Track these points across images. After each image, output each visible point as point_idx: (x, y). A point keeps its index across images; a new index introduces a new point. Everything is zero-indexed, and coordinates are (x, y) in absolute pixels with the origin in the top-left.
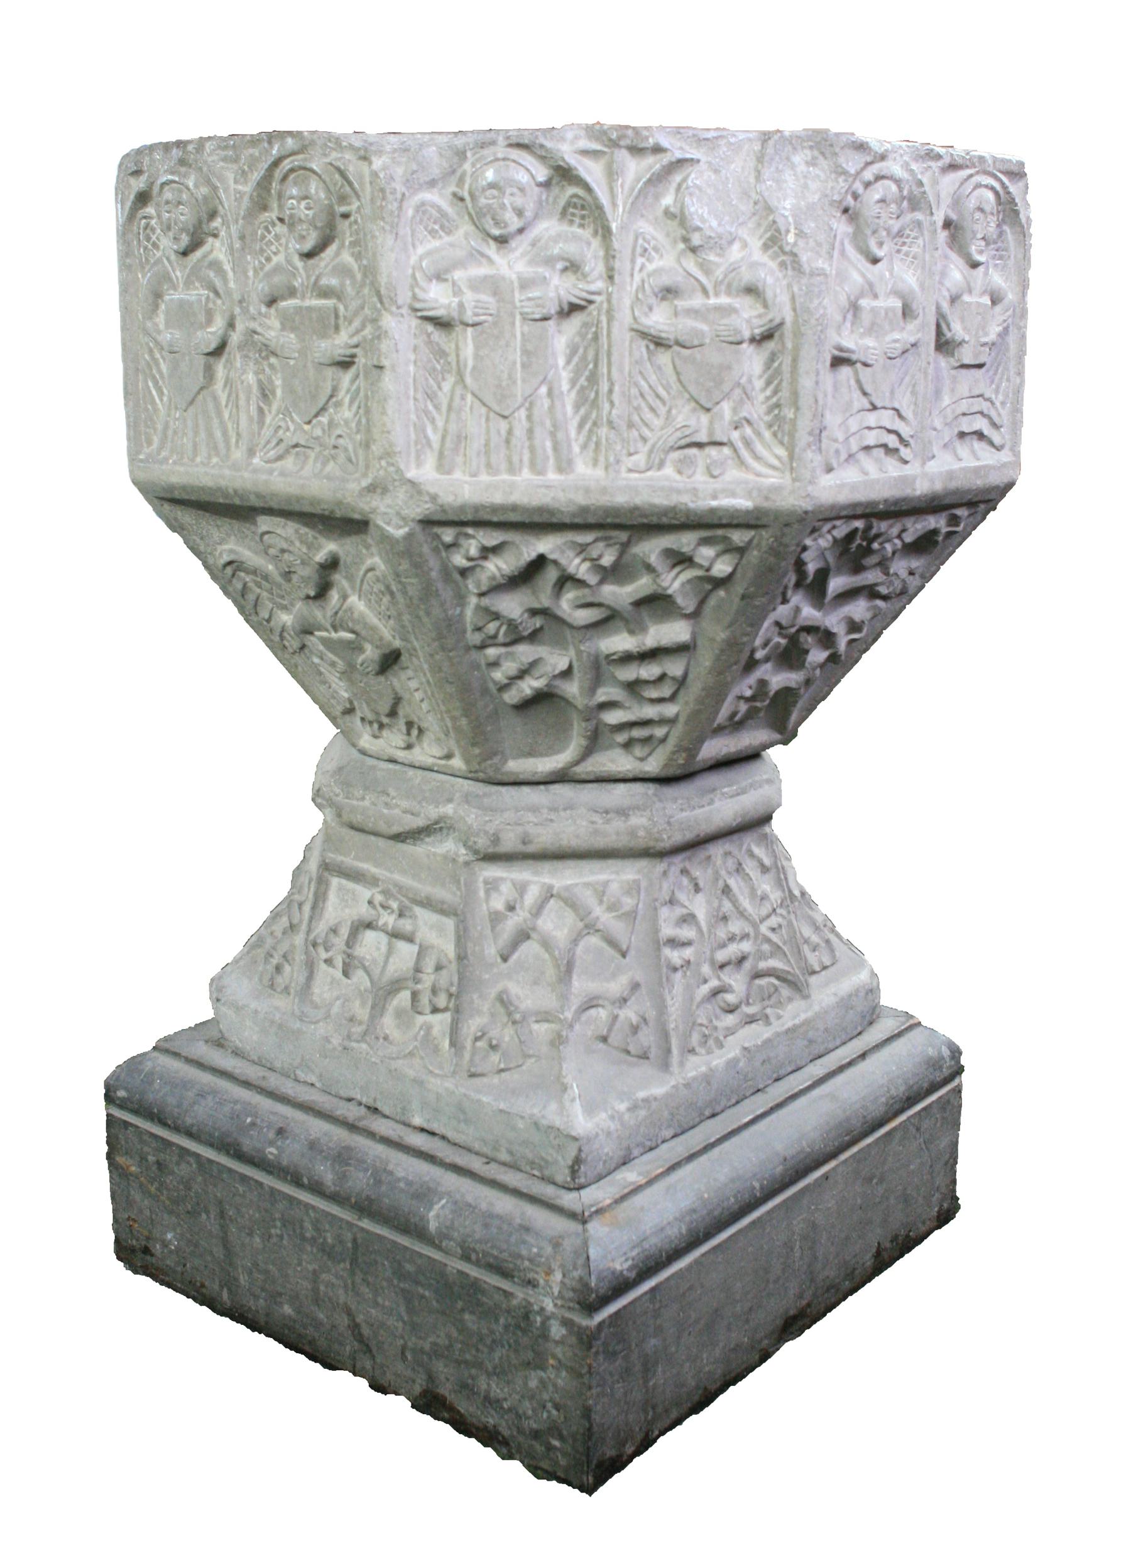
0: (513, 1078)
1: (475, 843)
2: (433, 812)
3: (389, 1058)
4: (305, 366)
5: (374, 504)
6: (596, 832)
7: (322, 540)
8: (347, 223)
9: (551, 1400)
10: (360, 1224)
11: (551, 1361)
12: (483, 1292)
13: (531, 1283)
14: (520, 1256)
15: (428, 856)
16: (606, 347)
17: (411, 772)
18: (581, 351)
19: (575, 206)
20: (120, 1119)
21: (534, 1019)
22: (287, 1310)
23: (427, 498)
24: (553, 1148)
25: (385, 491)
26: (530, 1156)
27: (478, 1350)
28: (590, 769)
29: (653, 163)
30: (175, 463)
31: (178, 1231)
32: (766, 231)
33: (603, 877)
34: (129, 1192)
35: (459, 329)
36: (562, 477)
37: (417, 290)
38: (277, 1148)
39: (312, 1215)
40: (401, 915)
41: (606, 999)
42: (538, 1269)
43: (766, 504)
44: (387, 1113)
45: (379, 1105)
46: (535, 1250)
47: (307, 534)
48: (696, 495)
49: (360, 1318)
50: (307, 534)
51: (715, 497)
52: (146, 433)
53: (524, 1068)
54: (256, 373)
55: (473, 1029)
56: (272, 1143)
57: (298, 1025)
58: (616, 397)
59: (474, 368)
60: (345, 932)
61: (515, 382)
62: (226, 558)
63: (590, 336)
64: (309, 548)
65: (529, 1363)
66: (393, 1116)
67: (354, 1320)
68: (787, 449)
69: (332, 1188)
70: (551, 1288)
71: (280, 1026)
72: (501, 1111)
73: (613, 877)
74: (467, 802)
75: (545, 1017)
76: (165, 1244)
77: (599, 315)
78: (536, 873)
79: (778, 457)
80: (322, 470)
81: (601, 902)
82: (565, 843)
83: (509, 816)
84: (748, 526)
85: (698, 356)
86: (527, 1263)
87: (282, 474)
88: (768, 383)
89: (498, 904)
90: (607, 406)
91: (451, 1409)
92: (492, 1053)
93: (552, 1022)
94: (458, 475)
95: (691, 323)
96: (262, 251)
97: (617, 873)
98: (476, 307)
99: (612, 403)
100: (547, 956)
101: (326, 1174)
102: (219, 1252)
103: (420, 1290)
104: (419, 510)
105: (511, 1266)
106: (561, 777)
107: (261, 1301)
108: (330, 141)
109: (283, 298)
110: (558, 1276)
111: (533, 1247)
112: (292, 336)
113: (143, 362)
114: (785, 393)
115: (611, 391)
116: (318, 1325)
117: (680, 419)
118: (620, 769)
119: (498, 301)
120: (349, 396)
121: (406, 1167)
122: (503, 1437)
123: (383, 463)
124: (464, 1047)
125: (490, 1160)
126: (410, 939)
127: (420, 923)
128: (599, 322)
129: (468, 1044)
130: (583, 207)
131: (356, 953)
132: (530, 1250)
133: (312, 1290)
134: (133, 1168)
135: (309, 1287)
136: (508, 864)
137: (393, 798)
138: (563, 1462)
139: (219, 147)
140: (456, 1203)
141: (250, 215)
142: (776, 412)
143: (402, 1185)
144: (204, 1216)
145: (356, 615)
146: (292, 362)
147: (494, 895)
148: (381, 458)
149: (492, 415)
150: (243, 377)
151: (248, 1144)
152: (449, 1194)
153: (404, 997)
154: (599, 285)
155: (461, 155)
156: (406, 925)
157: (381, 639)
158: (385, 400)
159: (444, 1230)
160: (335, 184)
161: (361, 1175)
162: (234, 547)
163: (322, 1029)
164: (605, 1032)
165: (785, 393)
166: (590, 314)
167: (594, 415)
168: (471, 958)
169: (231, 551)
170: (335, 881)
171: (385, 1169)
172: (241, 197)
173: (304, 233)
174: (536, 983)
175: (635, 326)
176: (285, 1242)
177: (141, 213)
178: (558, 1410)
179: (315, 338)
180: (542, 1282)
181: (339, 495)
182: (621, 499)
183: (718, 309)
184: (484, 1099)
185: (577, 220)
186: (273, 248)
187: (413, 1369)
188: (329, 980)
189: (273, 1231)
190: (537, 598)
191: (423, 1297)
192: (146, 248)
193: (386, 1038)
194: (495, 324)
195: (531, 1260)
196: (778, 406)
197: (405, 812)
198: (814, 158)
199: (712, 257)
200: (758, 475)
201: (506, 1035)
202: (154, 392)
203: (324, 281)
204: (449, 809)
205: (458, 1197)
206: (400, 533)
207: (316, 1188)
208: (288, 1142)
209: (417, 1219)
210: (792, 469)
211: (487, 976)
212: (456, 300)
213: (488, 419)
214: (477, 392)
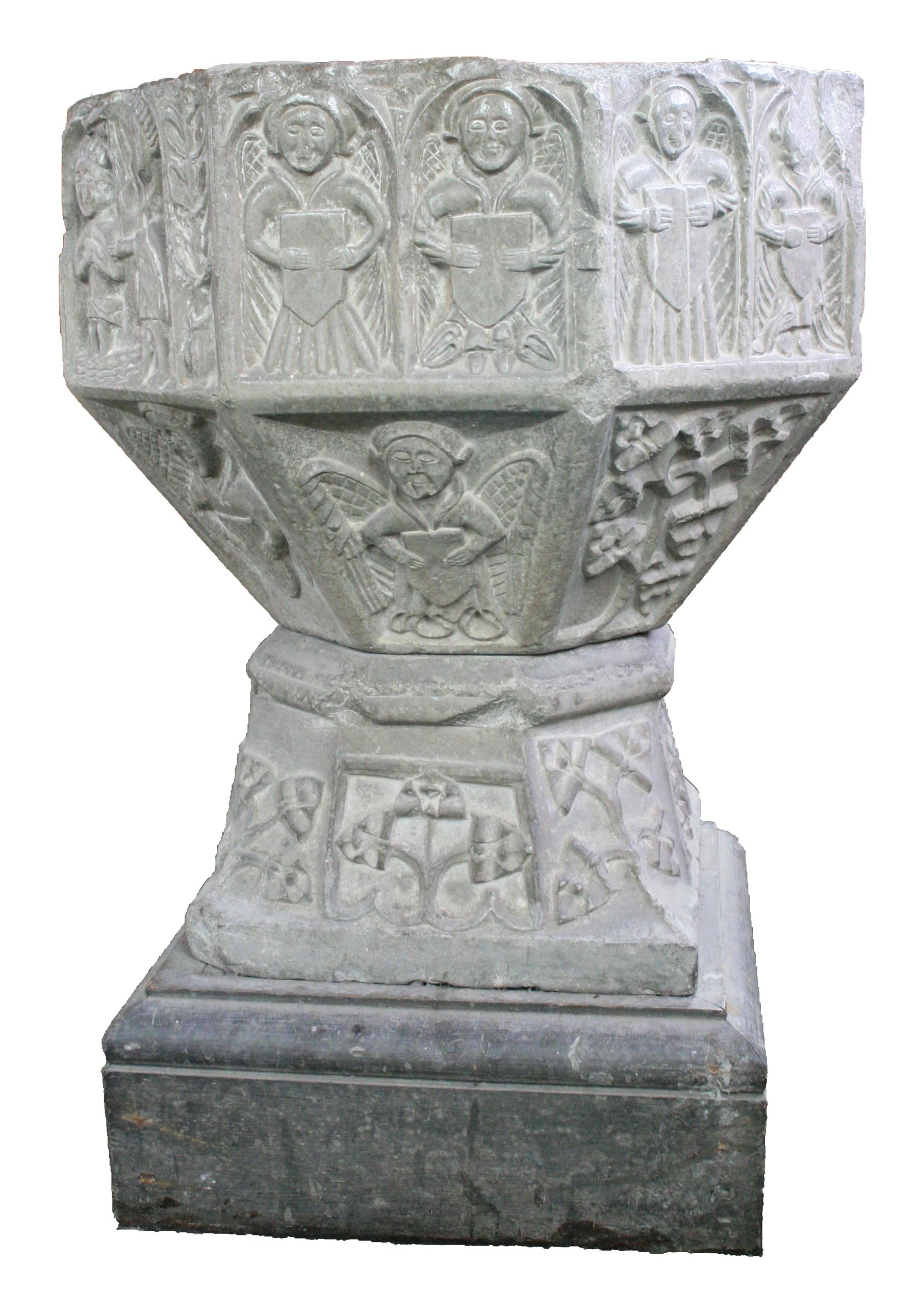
0: (601, 915)
1: (540, 709)
2: (495, 689)
3: (461, 930)
5: (580, 395)
6: (624, 684)
7: (462, 439)
8: (533, 142)
9: (719, 1184)
11: (721, 1147)
12: (639, 1108)
13: (699, 1083)
14: (681, 1062)
15: (480, 733)
16: (740, 249)
17: (447, 660)
18: (719, 252)
19: (715, 130)
20: (126, 1074)
21: (606, 859)
22: (379, 1203)
23: (629, 386)
24: (671, 963)
25: (593, 381)
26: (643, 977)
27: (631, 1164)
28: (612, 629)
29: (774, 93)
30: (297, 377)
31: (218, 1168)
32: (828, 151)
33: (622, 724)
34: (142, 1148)
35: (647, 235)
36: (714, 361)
37: (622, 201)
38: (363, 1045)
39: (416, 1097)
40: (449, 795)
41: (649, 830)
42: (704, 1067)
43: (837, 375)
44: (462, 983)
45: (450, 979)
47: (451, 434)
48: (797, 371)
49: (480, 1182)
50: (451, 434)
51: (808, 372)
52: (246, 352)
53: (609, 903)
54: (419, 284)
55: (552, 881)
56: (354, 1042)
57: (336, 927)
58: (749, 291)
59: (659, 268)
60: (376, 826)
61: (686, 281)
62: (316, 469)
63: (726, 240)
64: (452, 447)
65: (694, 1157)
66: (467, 985)
67: (472, 1186)
68: (844, 329)
69: (445, 1063)
70: (721, 1079)
71: (313, 933)
72: (608, 945)
73: (629, 723)
74: (527, 674)
75: (616, 855)
76: (196, 1188)
77: (734, 222)
78: (575, 731)
79: (838, 337)
80: (511, 368)
81: (626, 746)
82: (604, 698)
83: (561, 681)
84: (817, 395)
85: (796, 255)
87: (458, 376)
88: (828, 276)
89: (552, 764)
90: (740, 299)
91: (599, 1230)
92: (575, 898)
93: (622, 858)
94: (647, 364)
95: (792, 227)
96: (426, 168)
97: (631, 719)
98: (663, 216)
99: (746, 297)
100: (597, 802)
101: (435, 1054)
102: (279, 1174)
103: (560, 1130)
104: (619, 397)
106: (593, 641)
107: (341, 1205)
108: (524, 68)
109: (458, 211)
110: (727, 1067)
111: (688, 1053)
112: (472, 246)
113: (247, 281)
114: (843, 284)
115: (745, 286)
116: (421, 1204)
117: (784, 308)
118: (631, 626)
119: (675, 210)
120: (535, 300)
122: (663, 1236)
123: (596, 357)
124: (548, 899)
125: (597, 994)
126: (458, 816)
127: (467, 798)
128: (734, 227)
129: (551, 896)
130: (723, 130)
131: (392, 843)
132: (690, 1054)
133: (415, 1172)
134: (150, 1121)
135: (411, 1171)
136: (553, 726)
137: (443, 685)
138: (733, 1235)
139: (364, 71)
140: (591, 1036)
141: (416, 135)
142: (836, 299)
143: (524, 1038)
144: (258, 1142)
145: (473, 508)
146: (470, 271)
147: (548, 756)
148: (594, 352)
149: (671, 309)
150: (407, 288)
151: (324, 1050)
152: (578, 1031)
153: (461, 871)
154: (735, 197)
155: (646, 82)
156: (454, 803)
157: (495, 527)
158: (602, 299)
160: (532, 106)
161: (475, 1042)
162: (323, 459)
163: (368, 924)
164: (656, 859)
165: (843, 284)
166: (727, 220)
167: (729, 307)
168: (539, 817)
169: (322, 463)
170: (352, 780)
171: (498, 1031)
172: (404, 118)
173: (495, 151)
174: (594, 828)
175: (761, 230)
176: (377, 1136)
177: (247, 133)
178: (728, 1190)
180: (710, 1077)
181: (540, 390)
182: (752, 377)
183: (809, 215)
184: (586, 939)
185: (714, 141)
186: (437, 166)
187: (551, 1209)
188: (357, 876)
189: (360, 1129)
190: (656, 472)
191: (564, 1135)
192: (247, 168)
193: (445, 914)
194: (673, 230)
195: (694, 1063)
196: (838, 294)
197: (461, 694)
198: (843, 93)
199: (801, 173)
200: (828, 351)
201: (583, 879)
202: (257, 311)
203: (518, 194)
204: (512, 683)
205: (590, 1032)
206: (595, 420)
207: (425, 1071)
208: (372, 1036)
209: (556, 1063)
210: (850, 345)
211: (554, 831)
212: (648, 209)
213: (667, 313)
214: (661, 290)
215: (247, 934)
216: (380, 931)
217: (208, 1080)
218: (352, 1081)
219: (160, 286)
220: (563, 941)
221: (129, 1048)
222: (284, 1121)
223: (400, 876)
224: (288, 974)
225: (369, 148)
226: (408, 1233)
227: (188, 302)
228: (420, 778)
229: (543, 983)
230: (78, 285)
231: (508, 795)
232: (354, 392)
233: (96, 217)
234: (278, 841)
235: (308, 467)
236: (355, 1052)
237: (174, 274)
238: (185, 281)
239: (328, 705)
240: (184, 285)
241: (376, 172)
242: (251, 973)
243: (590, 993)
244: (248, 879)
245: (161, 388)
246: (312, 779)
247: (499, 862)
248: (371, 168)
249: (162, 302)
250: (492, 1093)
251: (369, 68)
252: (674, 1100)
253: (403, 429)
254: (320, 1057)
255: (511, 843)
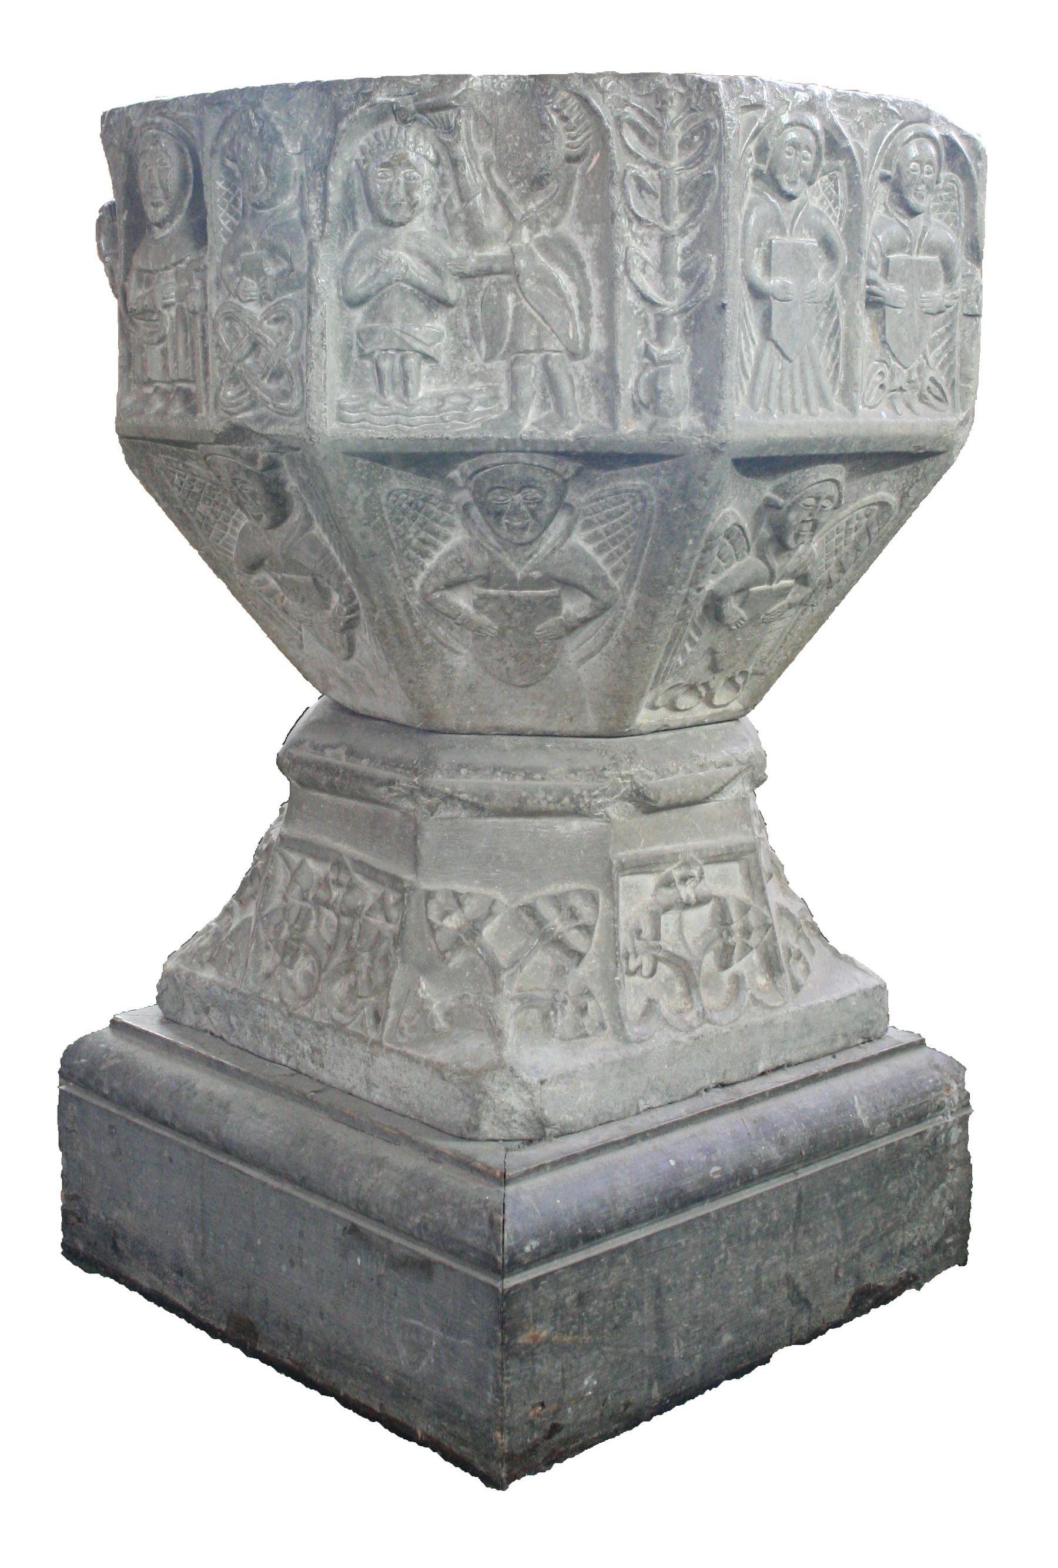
4: (911, 315)
10: (799, 1177)
17: (690, 732)
20: (525, 1284)
38: (717, 1164)
45: (730, 1078)
46: (931, 1081)
69: (781, 1158)
86: (933, 1094)
105: (925, 1105)
121: (810, 1099)
146: (899, 311)
159: (874, 1118)
179: (922, 289)
195: (935, 1090)
215: (566, 1083)
216: (677, 1043)
217: (598, 1258)
218: (709, 1208)
219: (571, 312)
220: (809, 1007)
221: (527, 1249)
222: (657, 1279)
223: (663, 980)
224: (601, 1119)
225: (831, 179)
226: (747, 1362)
227: (639, 332)
228: (679, 867)
229: (794, 1057)
230: (343, 309)
231: (735, 869)
232: (820, 433)
233: (408, 226)
234: (547, 972)
235: (724, 519)
236: (714, 1173)
237: (625, 300)
238: (636, 308)
239: (599, 801)
240: (635, 312)
241: (835, 204)
242: (568, 1130)
243: (825, 1055)
244: (530, 1024)
245: (570, 433)
246: (580, 891)
247: (745, 940)
248: (830, 199)
249: (574, 331)
250: (811, 1176)
251: (840, 98)
252: (925, 1132)
253: (825, 472)
254: (690, 1191)
255: (752, 919)
